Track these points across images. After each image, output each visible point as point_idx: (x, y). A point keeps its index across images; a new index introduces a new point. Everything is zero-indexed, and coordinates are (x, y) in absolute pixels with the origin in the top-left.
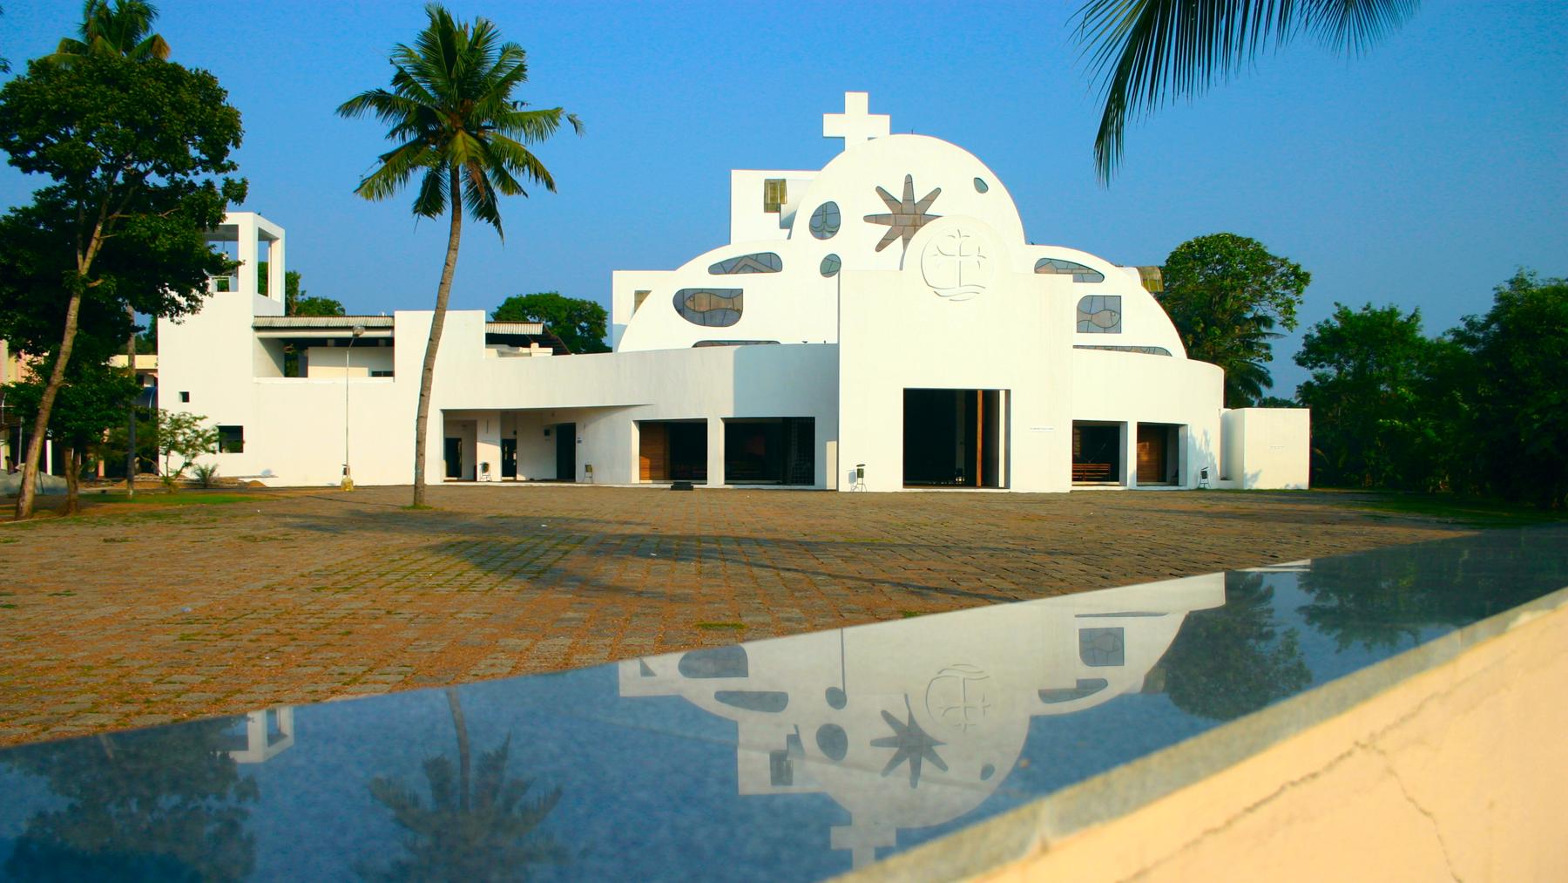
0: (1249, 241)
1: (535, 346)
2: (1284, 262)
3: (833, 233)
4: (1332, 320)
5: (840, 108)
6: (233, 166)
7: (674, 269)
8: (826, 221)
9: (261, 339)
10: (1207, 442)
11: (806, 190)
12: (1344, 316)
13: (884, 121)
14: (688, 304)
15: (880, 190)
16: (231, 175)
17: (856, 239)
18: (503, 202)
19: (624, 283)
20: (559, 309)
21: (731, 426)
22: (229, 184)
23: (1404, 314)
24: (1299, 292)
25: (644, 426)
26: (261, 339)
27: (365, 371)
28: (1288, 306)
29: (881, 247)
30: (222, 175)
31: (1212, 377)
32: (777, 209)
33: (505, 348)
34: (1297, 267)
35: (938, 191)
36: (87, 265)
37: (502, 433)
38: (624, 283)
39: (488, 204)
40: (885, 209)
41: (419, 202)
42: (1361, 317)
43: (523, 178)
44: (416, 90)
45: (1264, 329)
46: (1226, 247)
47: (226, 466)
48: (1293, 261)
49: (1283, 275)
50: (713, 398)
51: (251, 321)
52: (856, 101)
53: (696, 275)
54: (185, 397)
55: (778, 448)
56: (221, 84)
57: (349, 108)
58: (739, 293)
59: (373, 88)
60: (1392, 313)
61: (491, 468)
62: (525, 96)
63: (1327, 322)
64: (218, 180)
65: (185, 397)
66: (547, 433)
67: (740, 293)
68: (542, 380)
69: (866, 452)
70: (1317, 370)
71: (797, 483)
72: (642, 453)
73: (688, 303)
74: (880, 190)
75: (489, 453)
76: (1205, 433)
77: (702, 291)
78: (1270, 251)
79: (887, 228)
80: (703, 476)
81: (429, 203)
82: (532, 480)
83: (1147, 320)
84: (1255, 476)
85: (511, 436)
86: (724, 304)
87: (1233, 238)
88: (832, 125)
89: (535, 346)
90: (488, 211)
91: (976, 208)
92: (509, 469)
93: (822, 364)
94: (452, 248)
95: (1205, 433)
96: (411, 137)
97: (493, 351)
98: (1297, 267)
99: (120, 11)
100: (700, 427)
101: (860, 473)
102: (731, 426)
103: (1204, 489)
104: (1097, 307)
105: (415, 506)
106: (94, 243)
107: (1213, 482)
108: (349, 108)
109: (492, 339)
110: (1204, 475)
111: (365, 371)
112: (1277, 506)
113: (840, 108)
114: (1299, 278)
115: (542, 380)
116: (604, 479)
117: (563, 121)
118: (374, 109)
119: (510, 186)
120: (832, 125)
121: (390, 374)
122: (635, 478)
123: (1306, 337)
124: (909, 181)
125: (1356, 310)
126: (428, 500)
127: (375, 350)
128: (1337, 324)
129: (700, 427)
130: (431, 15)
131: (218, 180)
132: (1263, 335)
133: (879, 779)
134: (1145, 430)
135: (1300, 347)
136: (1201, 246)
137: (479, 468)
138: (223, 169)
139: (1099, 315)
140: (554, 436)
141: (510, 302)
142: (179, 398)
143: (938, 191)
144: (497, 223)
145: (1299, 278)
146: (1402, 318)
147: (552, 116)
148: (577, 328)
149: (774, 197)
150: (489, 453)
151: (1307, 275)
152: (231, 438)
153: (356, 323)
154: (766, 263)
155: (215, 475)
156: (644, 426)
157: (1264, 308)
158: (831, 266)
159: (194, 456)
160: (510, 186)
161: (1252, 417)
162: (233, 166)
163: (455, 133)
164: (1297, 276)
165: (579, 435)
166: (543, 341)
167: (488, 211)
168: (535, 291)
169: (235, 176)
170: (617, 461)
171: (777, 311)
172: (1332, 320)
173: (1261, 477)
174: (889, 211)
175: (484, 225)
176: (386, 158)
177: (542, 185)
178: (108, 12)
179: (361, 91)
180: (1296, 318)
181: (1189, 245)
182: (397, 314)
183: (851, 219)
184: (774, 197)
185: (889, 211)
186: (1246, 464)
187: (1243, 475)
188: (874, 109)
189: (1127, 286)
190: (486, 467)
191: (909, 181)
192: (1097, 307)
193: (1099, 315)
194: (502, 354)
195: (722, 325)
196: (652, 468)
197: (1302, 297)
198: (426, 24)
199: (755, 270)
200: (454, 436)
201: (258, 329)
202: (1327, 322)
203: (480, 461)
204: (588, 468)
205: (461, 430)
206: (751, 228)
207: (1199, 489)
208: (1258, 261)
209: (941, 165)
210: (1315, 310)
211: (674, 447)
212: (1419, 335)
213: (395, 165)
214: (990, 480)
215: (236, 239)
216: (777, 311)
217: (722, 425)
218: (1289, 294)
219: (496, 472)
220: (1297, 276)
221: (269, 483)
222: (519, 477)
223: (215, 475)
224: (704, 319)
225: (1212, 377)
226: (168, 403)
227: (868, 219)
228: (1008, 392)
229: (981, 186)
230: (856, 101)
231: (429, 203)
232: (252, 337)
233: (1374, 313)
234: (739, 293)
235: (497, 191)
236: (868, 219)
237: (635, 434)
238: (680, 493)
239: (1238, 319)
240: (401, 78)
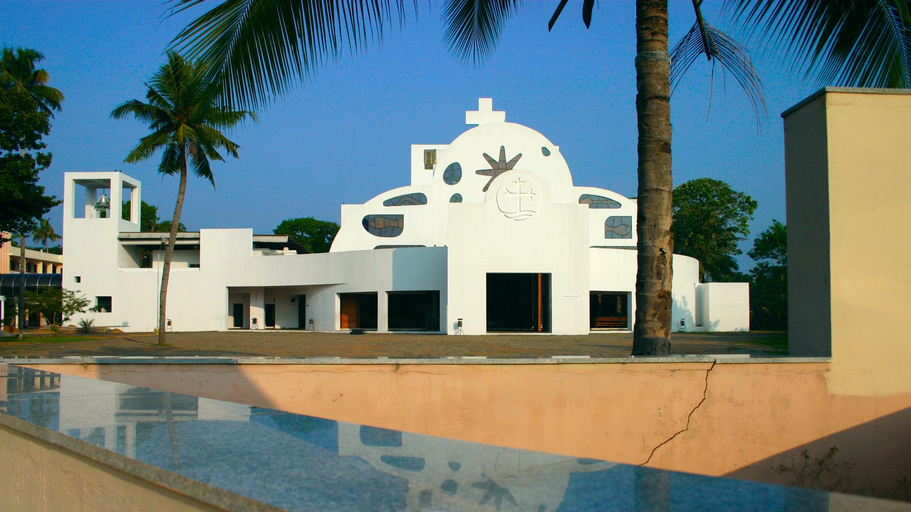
1: (286, 249)
2: (741, 195)
3: (458, 181)
4: (771, 230)
5: (476, 108)
6: (43, 146)
7: (363, 203)
8: (453, 174)
9: (124, 246)
10: (685, 303)
11: (446, 155)
13: (502, 115)
14: (369, 223)
15: (485, 155)
16: (42, 151)
17: (470, 184)
18: (213, 164)
19: (346, 209)
20: (313, 227)
21: (393, 297)
22: (40, 156)
24: (751, 213)
25: (344, 297)
26: (124, 246)
27: (186, 264)
28: (744, 221)
30: (37, 151)
33: (267, 250)
34: (748, 198)
35: (520, 155)
37: (265, 299)
38: (346, 209)
43: (221, 150)
44: (160, 99)
46: (705, 186)
47: (101, 320)
48: (746, 195)
49: (741, 203)
50: (381, 282)
51: (117, 235)
52: (485, 103)
53: (376, 206)
54: (78, 279)
55: (418, 310)
57: (118, 113)
58: (401, 217)
59: (130, 98)
61: (258, 321)
64: (34, 153)
65: (78, 279)
66: (293, 301)
67: (402, 217)
68: (289, 269)
69: (466, 309)
70: (761, 261)
71: (431, 330)
72: (342, 312)
74: (485, 155)
75: (257, 312)
76: (684, 298)
77: (379, 216)
78: (732, 188)
80: (374, 326)
82: (284, 329)
84: (716, 323)
85: (271, 303)
86: (393, 224)
87: (710, 181)
88: (471, 117)
89: (286, 249)
90: (205, 170)
91: (543, 168)
92: (270, 321)
94: (182, 192)
95: (684, 298)
97: (259, 253)
98: (748, 198)
99: (20, 57)
100: (372, 298)
101: (460, 324)
102: (393, 297)
103: (683, 332)
104: (617, 223)
105: (160, 344)
107: (690, 327)
108: (118, 113)
109: (257, 245)
110: (683, 323)
111: (186, 264)
112: (704, 342)
114: (750, 205)
115: (289, 269)
116: (320, 328)
117: (247, 115)
118: (133, 113)
119: (216, 156)
121: (198, 266)
122: (337, 327)
124: (503, 150)
126: (168, 341)
129: (372, 298)
130: (170, 56)
131: (34, 153)
133: (476, 505)
136: (690, 186)
137: (251, 321)
138: (36, 147)
141: (284, 223)
142: (74, 280)
143: (520, 155)
144: (211, 178)
148: (313, 236)
149: (430, 160)
150: (257, 312)
151: (755, 202)
152: (105, 303)
153: (183, 237)
154: (419, 199)
155: (92, 325)
156: (344, 297)
157: (731, 223)
159: (72, 314)
160: (216, 156)
161: (714, 288)
162: (43, 146)
163: (180, 125)
164: (750, 203)
165: (308, 302)
166: (291, 245)
167: (205, 170)
168: (299, 217)
169: (44, 152)
170: (329, 316)
171: (419, 228)
172: (771, 230)
173: (720, 324)
174: (491, 168)
175: (204, 179)
178: (13, 57)
179: (123, 102)
181: (684, 186)
182: (202, 231)
183: (468, 173)
184: (430, 160)
185: (491, 168)
186: (710, 316)
187: (709, 323)
188: (495, 108)
190: (255, 321)
191: (503, 150)
192: (617, 223)
194: (266, 254)
196: (350, 321)
197: (753, 216)
198: (165, 61)
199: (411, 204)
201: (121, 239)
202: (768, 231)
203: (252, 317)
204: (311, 321)
205: (239, 301)
206: (422, 179)
207: (680, 332)
208: (725, 193)
209: (525, 141)
211: (359, 308)
213: (147, 146)
214: (547, 327)
215: (109, 187)
216: (419, 228)
217: (386, 296)
218: (746, 214)
219: (261, 325)
220: (750, 203)
221: (125, 330)
222: (277, 327)
223: (92, 325)
224: (380, 233)
226: (68, 284)
227: (478, 172)
229: (546, 152)
230: (485, 103)
232: (117, 245)
234: (401, 217)
235: (208, 157)
236: (478, 172)
238: (356, 336)
239: (719, 231)
240: (151, 94)
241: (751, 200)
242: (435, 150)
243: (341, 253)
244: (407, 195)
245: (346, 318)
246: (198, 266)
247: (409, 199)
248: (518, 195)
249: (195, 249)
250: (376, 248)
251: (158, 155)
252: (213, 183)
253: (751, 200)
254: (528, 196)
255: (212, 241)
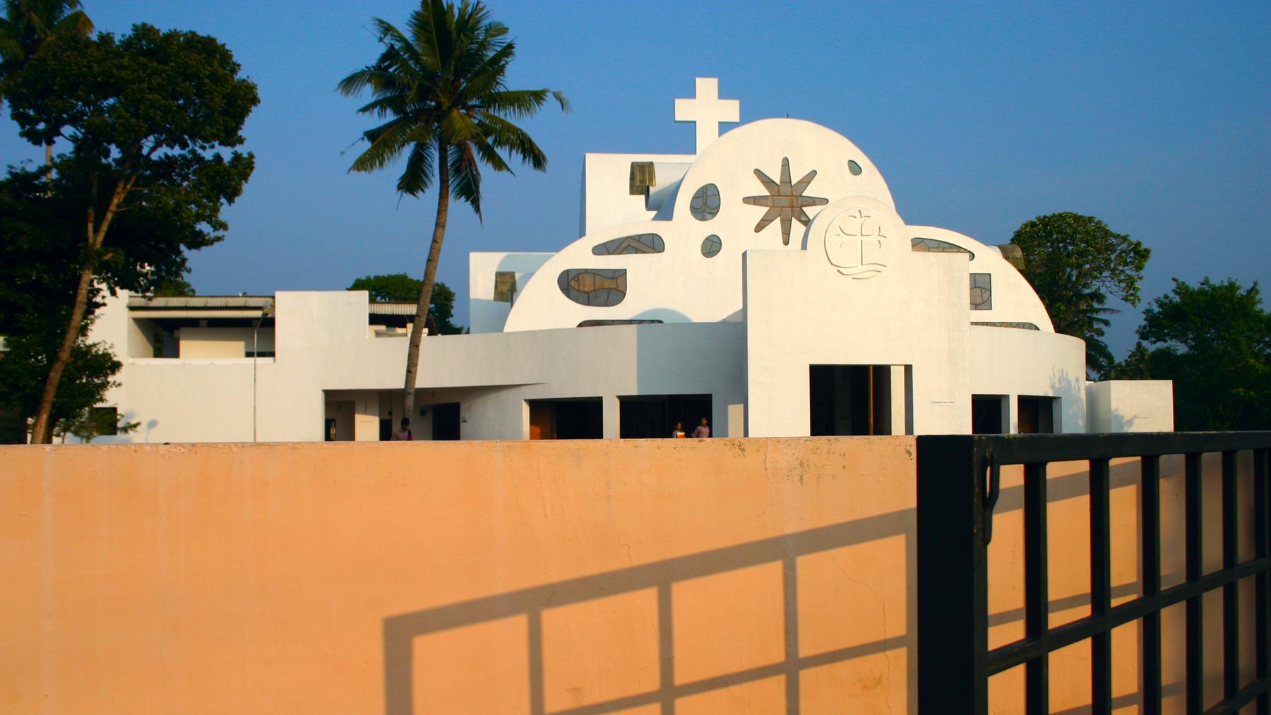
0: (1091, 219)
2: (1125, 238)
5: (691, 93)
8: (706, 203)
12: (1182, 290)
14: (572, 284)
15: (758, 173)
17: (736, 220)
23: (1244, 286)
24: (1139, 268)
25: (535, 405)
26: (138, 321)
28: (1130, 283)
29: (759, 228)
31: (1075, 348)
32: (646, 191)
33: (382, 328)
34: (1139, 244)
36: (101, 238)
39: (468, 184)
40: (808, 192)
41: (403, 178)
42: (1201, 292)
45: (1096, 305)
46: (1070, 226)
48: (1133, 239)
49: (1123, 251)
52: (707, 86)
53: (578, 256)
56: (236, 58)
60: (1232, 287)
62: (513, 79)
63: (1166, 297)
66: (423, 413)
72: (532, 422)
73: (572, 283)
74: (758, 173)
77: (586, 271)
78: (1113, 228)
79: (778, 221)
81: (412, 181)
83: (1017, 297)
85: (387, 417)
86: (607, 284)
88: (684, 110)
93: (733, 336)
94: (440, 224)
96: (390, 117)
98: (1139, 244)
106: (109, 216)
109: (375, 319)
113: (691, 93)
114: (1140, 254)
117: (550, 98)
119: (499, 164)
120: (684, 110)
121: (272, 354)
123: (1148, 312)
124: (786, 164)
125: (1194, 285)
127: (258, 332)
128: (1177, 299)
132: (1097, 311)
134: (1023, 400)
135: (1141, 321)
136: (1045, 225)
139: (981, 291)
140: (429, 419)
145: (1140, 254)
146: (1242, 292)
147: (538, 96)
151: (1147, 251)
156: (535, 405)
158: (712, 247)
165: (464, 414)
167: (470, 191)
169: (242, 150)
172: (1171, 295)
174: (767, 193)
176: (371, 135)
177: (529, 164)
180: (1138, 294)
181: (1033, 225)
184: (641, 180)
185: (767, 193)
189: (991, 261)
191: (786, 164)
193: (981, 291)
195: (606, 305)
197: (1142, 273)
199: (637, 251)
200: (331, 417)
202: (1166, 297)
205: (340, 410)
209: (813, 149)
210: (1156, 285)
212: (1258, 307)
213: (381, 142)
217: (617, 403)
218: (1129, 271)
225: (1075, 348)
228: (908, 369)
229: (855, 168)
230: (707, 86)
231: (412, 181)
233: (1214, 288)
237: (526, 409)
241: (1142, 247)
242: (651, 164)
243: (534, 333)
244: (630, 237)
245: (538, 430)
246: (272, 354)
247: (634, 244)
248: (859, 238)
249: (268, 323)
250: (580, 325)
251: (399, 163)
252: (478, 210)
253: (1142, 247)
254: (874, 239)
255: (296, 312)
